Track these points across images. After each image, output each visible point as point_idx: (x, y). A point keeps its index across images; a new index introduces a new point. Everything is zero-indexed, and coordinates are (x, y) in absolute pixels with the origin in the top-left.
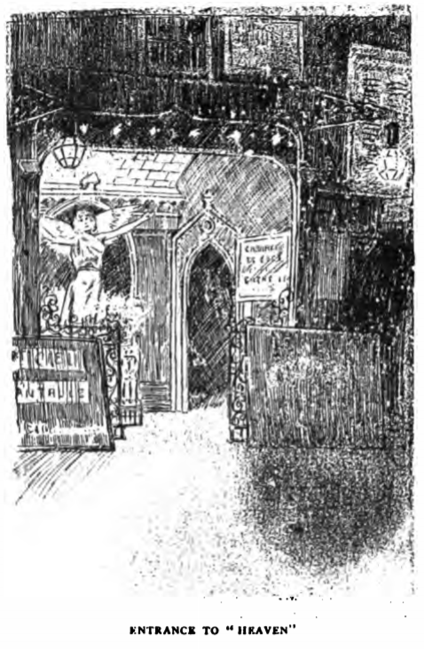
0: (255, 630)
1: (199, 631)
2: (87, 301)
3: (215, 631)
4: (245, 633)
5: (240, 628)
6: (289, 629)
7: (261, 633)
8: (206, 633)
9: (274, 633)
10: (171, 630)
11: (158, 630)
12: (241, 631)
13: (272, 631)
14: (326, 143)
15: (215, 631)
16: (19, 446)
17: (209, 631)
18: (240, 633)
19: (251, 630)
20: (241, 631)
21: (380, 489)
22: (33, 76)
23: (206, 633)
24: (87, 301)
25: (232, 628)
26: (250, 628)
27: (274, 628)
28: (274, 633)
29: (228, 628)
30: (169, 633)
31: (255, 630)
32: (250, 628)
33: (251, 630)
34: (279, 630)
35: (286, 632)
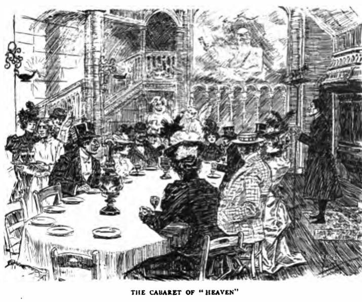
0: (215, 292)
1: (183, 293)
2: (14, 17)
3: (188, 292)
4: (139, 294)
5: (207, 291)
6: (234, 292)
7: (219, 294)
8: (133, 294)
9: (226, 294)
10: (158, 292)
11: (226, 293)
12: (208, 293)
13: (225, 292)
14: (183, 187)
15: (188, 292)
16: (290, 7)
17: (135, 293)
18: (207, 294)
19: (170, 292)
20: (208, 293)
21: (256, 258)
22: (259, 134)
23: (133, 294)
24: (14, 17)
25: (202, 291)
26: (212, 291)
27: (226, 291)
28: (226, 294)
29: (200, 291)
30: (157, 294)
31: (215, 292)
32: (212, 291)
33: (213, 292)
34: (229, 292)
35: (233, 293)
